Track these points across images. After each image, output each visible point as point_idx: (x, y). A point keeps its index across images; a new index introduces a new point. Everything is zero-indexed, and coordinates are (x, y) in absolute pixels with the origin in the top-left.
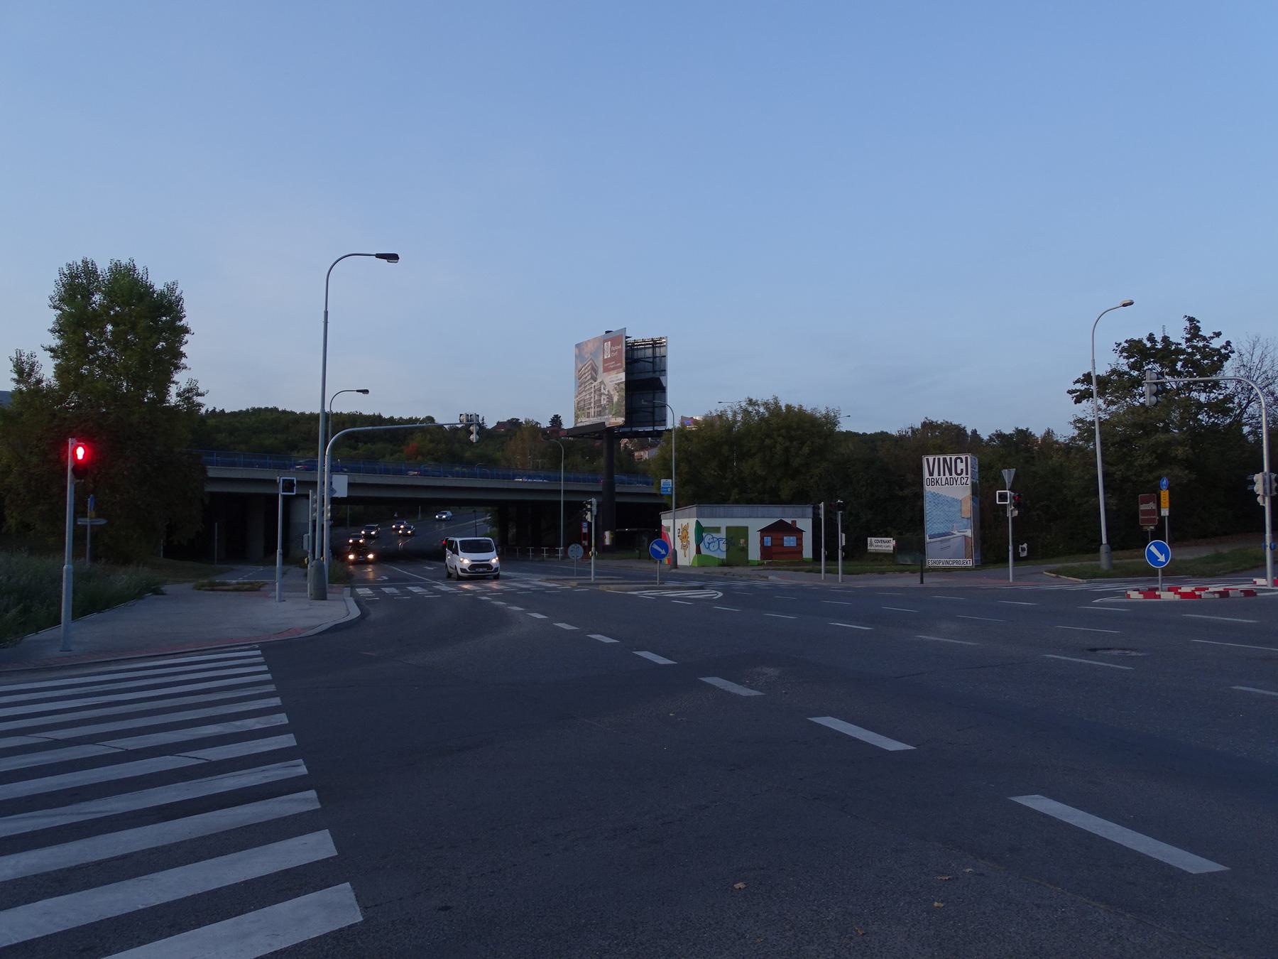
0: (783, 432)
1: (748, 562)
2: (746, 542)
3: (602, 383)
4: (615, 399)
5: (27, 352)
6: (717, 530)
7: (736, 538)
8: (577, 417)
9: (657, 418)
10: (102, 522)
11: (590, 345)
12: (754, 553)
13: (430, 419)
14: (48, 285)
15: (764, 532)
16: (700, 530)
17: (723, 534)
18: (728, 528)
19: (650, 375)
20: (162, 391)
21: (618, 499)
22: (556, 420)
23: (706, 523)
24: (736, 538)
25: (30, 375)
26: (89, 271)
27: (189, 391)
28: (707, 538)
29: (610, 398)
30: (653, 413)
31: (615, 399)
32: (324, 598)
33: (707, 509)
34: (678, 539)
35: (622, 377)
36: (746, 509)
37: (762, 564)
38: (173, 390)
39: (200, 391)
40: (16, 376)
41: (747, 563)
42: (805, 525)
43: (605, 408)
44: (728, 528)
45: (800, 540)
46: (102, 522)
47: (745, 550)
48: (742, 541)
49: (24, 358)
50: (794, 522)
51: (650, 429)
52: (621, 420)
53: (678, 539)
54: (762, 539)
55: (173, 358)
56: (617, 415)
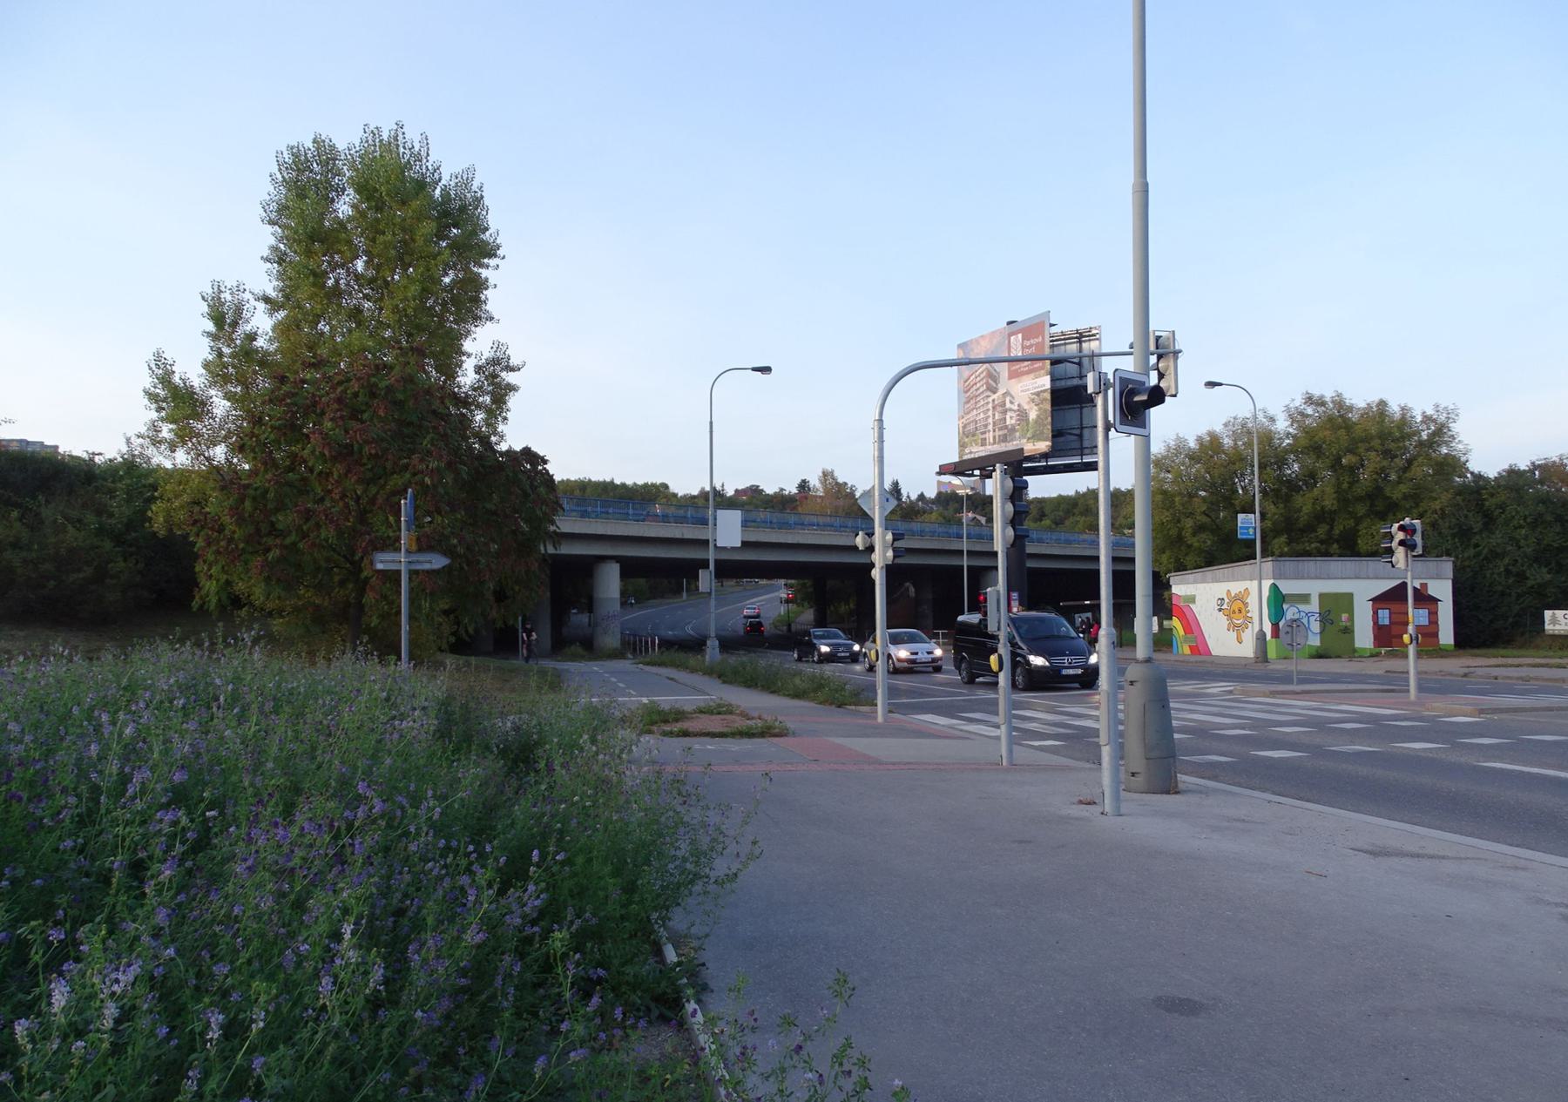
0: (1376, 443)
1: (1355, 650)
2: (1351, 618)
3: (1007, 393)
4: (1033, 415)
5: (230, 282)
6: (1305, 598)
7: (1335, 610)
8: (962, 446)
9: (1086, 444)
10: (437, 562)
11: (984, 343)
12: (1364, 637)
13: (666, 486)
14: (261, 184)
15: (1379, 601)
16: (1278, 600)
17: (1314, 606)
18: (1321, 596)
19: (1076, 382)
20: (450, 368)
21: (1030, 564)
22: (803, 485)
23: (1287, 587)
24: (1335, 610)
25: (235, 324)
26: (326, 153)
27: (495, 362)
28: (1290, 612)
29: (1022, 414)
30: (1081, 436)
31: (1033, 415)
32: (1170, 788)
33: (1290, 565)
34: (1255, 615)
35: (1045, 382)
36: (1349, 565)
37: (1378, 655)
38: (469, 365)
39: (514, 362)
40: (210, 326)
41: (1352, 653)
42: (1442, 590)
43: (1013, 430)
44: (1321, 596)
45: (1433, 615)
46: (437, 562)
47: (1348, 631)
48: (1344, 616)
49: (227, 296)
50: (1424, 586)
51: (1076, 460)
52: (1044, 446)
53: (1255, 615)
54: (1375, 613)
55: (468, 301)
56: (1036, 437)
